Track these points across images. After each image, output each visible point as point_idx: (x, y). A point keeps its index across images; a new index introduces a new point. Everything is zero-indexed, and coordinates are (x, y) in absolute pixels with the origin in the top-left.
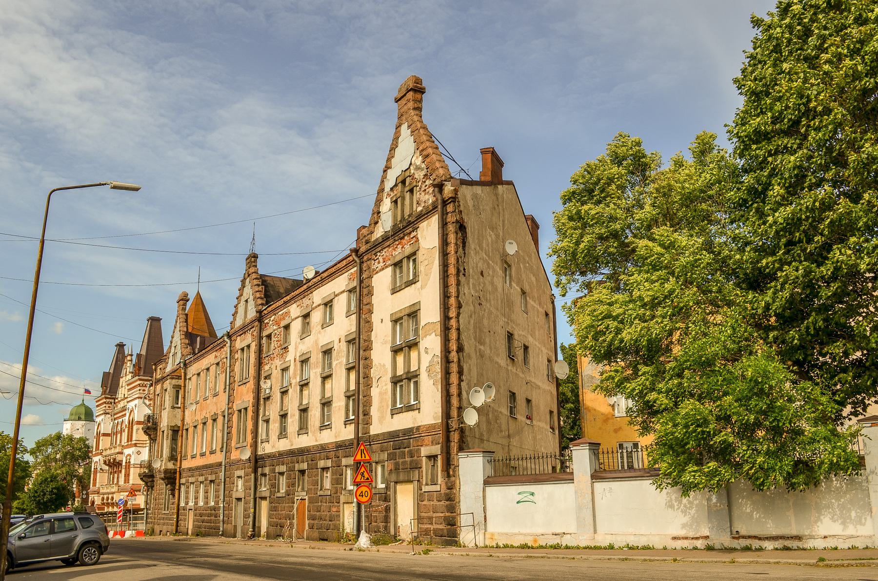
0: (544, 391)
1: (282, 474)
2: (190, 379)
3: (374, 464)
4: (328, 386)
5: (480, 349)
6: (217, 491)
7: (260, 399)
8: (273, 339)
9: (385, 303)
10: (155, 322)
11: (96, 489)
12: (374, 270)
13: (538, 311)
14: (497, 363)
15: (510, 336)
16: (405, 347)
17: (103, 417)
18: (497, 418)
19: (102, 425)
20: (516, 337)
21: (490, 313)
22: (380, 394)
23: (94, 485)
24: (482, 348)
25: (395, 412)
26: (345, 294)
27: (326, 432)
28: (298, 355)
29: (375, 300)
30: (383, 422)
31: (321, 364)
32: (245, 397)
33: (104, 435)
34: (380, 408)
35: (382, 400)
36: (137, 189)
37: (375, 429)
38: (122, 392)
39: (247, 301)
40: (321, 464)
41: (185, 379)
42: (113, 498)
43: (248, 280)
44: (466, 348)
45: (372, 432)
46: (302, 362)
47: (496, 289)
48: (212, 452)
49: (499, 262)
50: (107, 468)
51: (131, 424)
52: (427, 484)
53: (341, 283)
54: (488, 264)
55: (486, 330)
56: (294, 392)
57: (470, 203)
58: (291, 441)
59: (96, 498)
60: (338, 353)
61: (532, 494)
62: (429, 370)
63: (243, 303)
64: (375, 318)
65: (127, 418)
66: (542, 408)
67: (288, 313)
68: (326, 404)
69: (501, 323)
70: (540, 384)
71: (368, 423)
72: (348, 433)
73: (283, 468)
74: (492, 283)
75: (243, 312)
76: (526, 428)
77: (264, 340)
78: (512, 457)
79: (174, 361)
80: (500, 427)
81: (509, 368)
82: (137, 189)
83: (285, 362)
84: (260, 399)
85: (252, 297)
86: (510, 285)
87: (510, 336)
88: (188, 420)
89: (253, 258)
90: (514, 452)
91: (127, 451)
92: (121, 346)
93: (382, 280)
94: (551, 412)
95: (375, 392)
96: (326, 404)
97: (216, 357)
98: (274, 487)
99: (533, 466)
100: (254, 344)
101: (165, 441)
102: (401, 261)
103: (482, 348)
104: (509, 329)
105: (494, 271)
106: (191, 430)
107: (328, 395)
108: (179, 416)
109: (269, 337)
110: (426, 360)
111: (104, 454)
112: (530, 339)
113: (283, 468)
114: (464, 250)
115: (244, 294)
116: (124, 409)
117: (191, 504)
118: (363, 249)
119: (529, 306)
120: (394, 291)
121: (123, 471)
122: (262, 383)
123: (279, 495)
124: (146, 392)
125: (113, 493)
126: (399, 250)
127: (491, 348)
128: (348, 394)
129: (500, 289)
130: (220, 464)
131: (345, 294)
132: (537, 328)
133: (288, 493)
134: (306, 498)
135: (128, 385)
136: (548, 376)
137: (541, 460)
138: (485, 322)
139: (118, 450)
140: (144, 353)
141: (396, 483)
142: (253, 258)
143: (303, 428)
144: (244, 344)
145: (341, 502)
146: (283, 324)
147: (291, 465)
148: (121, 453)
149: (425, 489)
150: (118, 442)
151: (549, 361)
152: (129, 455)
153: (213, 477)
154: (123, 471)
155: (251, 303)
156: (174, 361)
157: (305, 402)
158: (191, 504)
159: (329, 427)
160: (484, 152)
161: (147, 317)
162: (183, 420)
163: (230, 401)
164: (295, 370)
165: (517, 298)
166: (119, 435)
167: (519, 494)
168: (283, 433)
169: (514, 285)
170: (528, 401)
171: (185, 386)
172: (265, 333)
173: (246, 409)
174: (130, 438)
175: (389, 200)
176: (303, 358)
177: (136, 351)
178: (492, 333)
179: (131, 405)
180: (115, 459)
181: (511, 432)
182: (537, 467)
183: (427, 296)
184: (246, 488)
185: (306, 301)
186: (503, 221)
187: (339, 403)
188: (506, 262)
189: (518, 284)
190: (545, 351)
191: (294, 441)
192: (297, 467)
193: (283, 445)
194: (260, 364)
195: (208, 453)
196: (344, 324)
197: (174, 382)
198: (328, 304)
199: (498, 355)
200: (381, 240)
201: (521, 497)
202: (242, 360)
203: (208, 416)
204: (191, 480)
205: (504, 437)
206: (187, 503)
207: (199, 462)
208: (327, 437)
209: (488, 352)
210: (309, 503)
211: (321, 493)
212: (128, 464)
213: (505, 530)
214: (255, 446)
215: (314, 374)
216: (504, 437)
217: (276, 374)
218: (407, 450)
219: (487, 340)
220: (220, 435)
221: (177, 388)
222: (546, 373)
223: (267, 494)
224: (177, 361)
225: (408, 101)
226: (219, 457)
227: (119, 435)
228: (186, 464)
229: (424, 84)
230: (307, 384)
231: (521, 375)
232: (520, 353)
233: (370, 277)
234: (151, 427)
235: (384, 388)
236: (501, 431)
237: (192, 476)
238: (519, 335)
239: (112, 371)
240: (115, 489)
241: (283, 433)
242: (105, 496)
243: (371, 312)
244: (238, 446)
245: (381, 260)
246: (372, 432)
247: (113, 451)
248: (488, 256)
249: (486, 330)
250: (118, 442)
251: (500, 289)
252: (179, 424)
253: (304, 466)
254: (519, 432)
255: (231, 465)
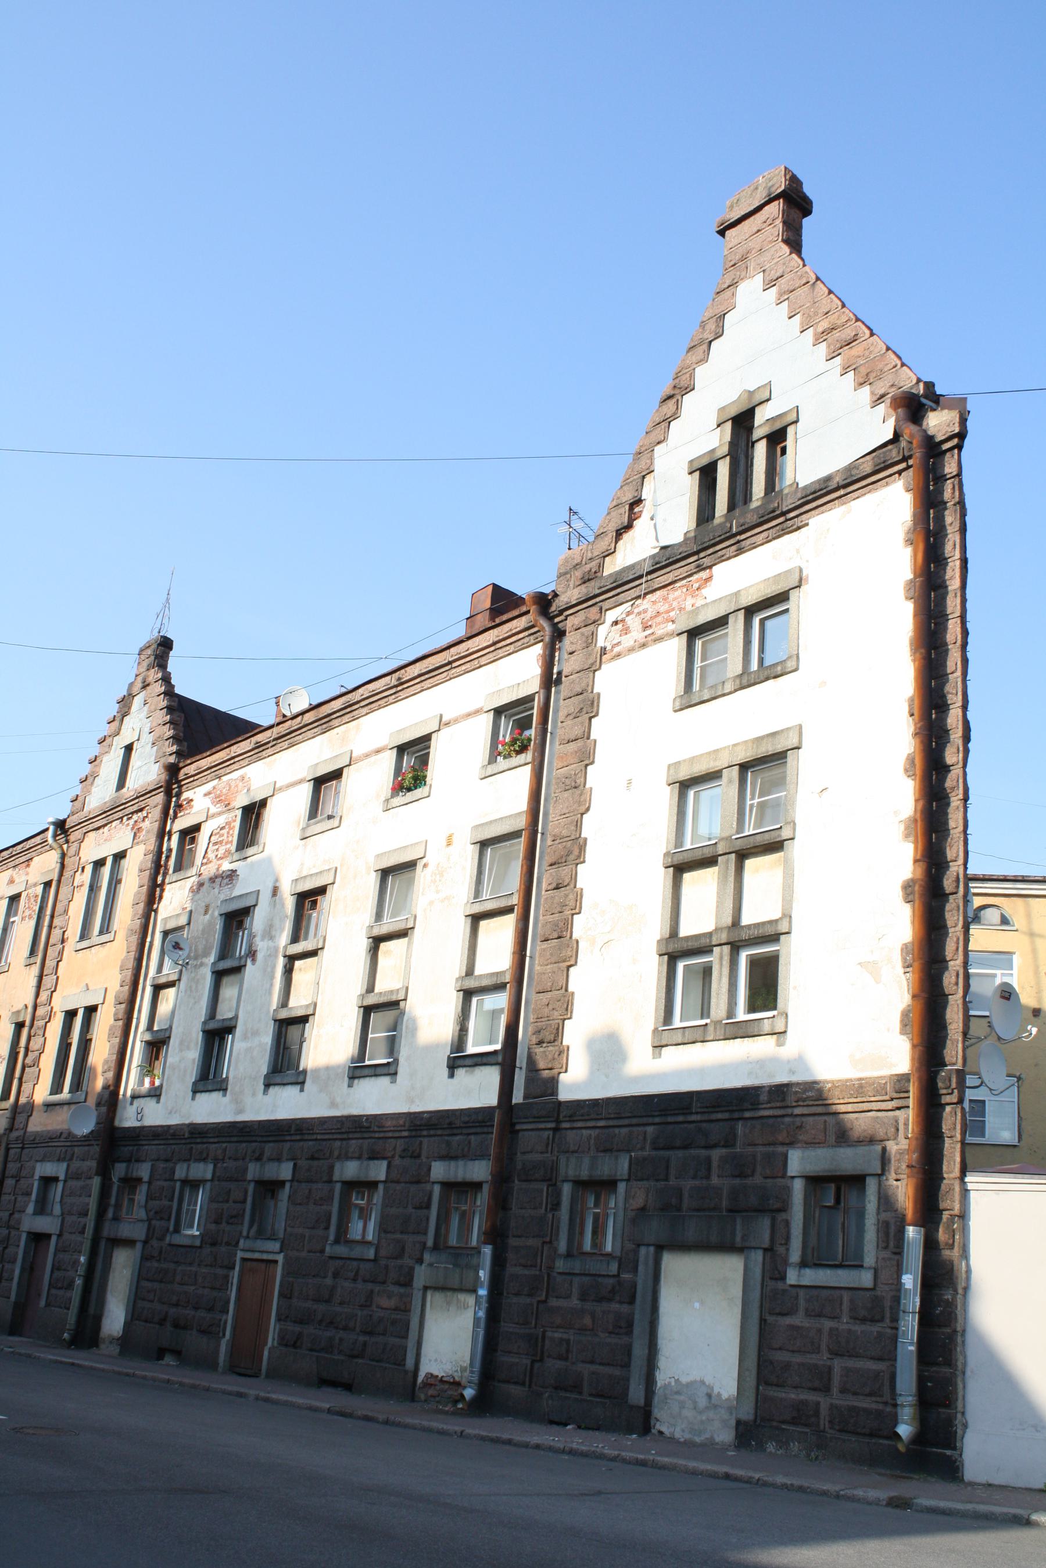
1: (193, 1185)
3: (567, 1189)
4: (229, 992)
12: (604, 651)
39: (129, 748)
40: (350, 1170)
43: (138, 701)
46: (385, 873)
52: (804, 1264)
58: (237, 1101)
97: (11, 881)
98: (165, 1216)
107: (224, 1012)
109: (190, 833)
113: (203, 1170)
118: (570, 595)
123: (177, 1240)
128: (471, 984)
133: (209, 1240)
134: (280, 1258)
141: (660, 1248)
144: (107, 850)
145: (419, 1281)
147: (230, 1164)
172: (183, 822)
173: (91, 1010)
192: (180, 1172)
193: (210, 1110)
196: (477, 792)
200: (647, 568)
210: (286, 1273)
211: (341, 1250)
218: (716, 1154)
223: (138, 1232)
229: (808, 190)
230: (238, 970)
243: (586, 758)
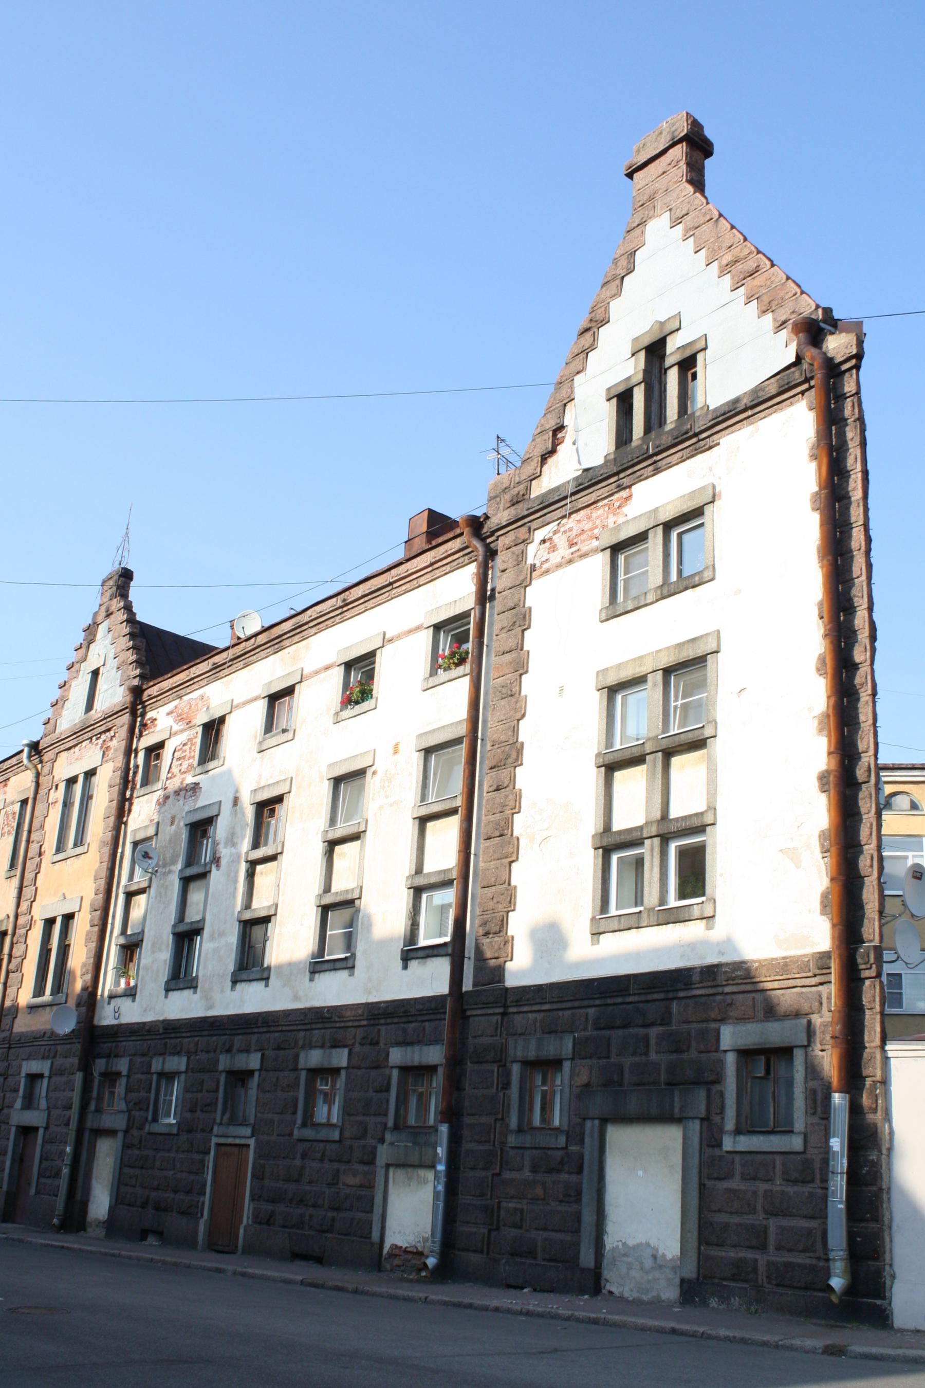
134: (252, 1142)
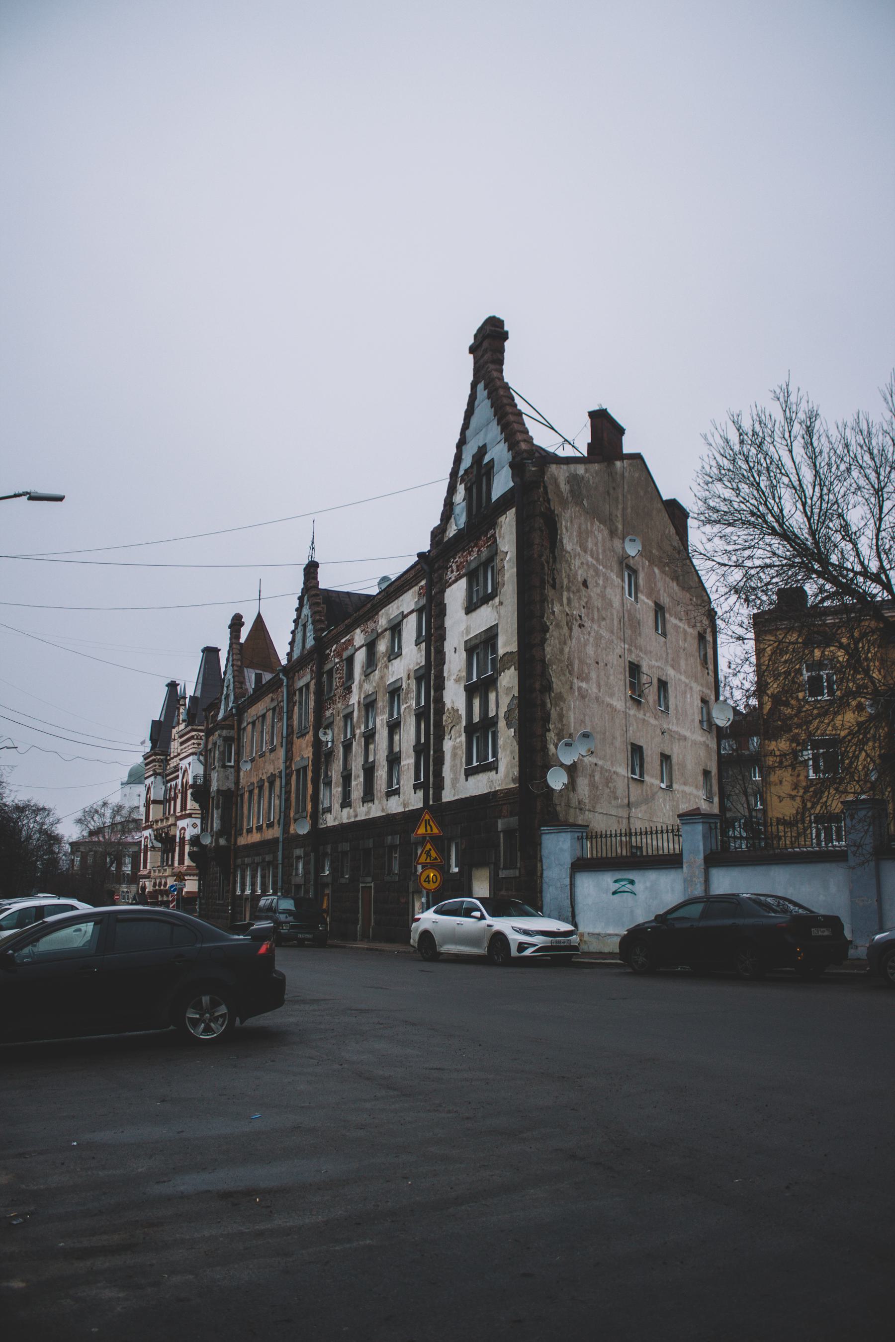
0: (695, 743)
2: (244, 729)
5: (580, 688)
6: (275, 876)
7: (322, 756)
8: (335, 676)
9: (460, 626)
10: (210, 653)
11: (146, 872)
13: (685, 632)
14: (611, 706)
15: (634, 669)
16: (479, 688)
17: (152, 779)
18: (608, 781)
19: (152, 789)
20: (645, 669)
21: (598, 638)
22: (455, 748)
23: (145, 867)
24: (584, 685)
25: (470, 772)
26: (414, 615)
27: (394, 800)
28: (362, 696)
29: (448, 622)
30: (459, 786)
31: (387, 710)
32: (304, 750)
33: (155, 802)
34: (453, 767)
35: (454, 755)
36: (60, 499)
37: (448, 796)
38: (175, 746)
41: (239, 729)
42: (166, 884)
44: (555, 686)
45: (444, 800)
47: (611, 605)
48: (270, 825)
49: (616, 567)
50: (160, 845)
51: (185, 787)
52: (505, 868)
53: (408, 601)
54: (597, 571)
55: (591, 661)
56: (357, 748)
57: (564, 487)
58: (355, 811)
59: (147, 883)
60: (407, 693)
61: (632, 882)
62: (507, 716)
63: (300, 628)
64: (448, 647)
65: (179, 781)
66: (690, 765)
67: (350, 642)
68: (394, 760)
69: (618, 651)
70: (688, 734)
71: (439, 785)
72: (414, 800)
73: (346, 847)
74: (603, 596)
75: (301, 641)
76: (660, 794)
77: (325, 678)
78: (633, 831)
79: (227, 705)
80: (614, 792)
81: (632, 712)
82: (60, 499)
83: (348, 706)
84: (322, 756)
85: (310, 620)
86: (636, 598)
87: (634, 669)
88: (243, 782)
89: (311, 569)
90: (637, 825)
91: (181, 824)
92: (172, 686)
93: (456, 594)
94: (706, 773)
95: (448, 745)
96: (394, 760)
97: (272, 700)
99: (660, 844)
100: (313, 682)
101: (215, 811)
102: (476, 569)
103: (584, 685)
104: (633, 658)
105: (606, 579)
106: (246, 795)
108: (232, 778)
110: (505, 702)
111: (155, 827)
112: (671, 672)
113: (346, 847)
114: (553, 552)
115: (302, 616)
116: (176, 769)
117: (248, 892)
119: (669, 627)
120: (470, 608)
121: (177, 848)
122: (321, 734)
123: (343, 881)
124: (202, 746)
125: (166, 877)
126: (475, 554)
127: (599, 686)
129: (616, 603)
130: (275, 841)
131: (414, 615)
132: (682, 655)
134: (372, 885)
135: (181, 737)
136: (701, 722)
137: (659, 836)
138: (590, 650)
139: (171, 821)
140: (198, 694)
142: (311, 569)
143: (368, 796)
145: (411, 890)
146: (345, 655)
148: (175, 825)
149: (503, 874)
150: (172, 812)
151: (704, 701)
152: (183, 828)
153: (268, 858)
154: (177, 848)
155: (310, 627)
156: (227, 705)
157: (371, 759)
158: (248, 892)
159: (397, 792)
160: (593, 415)
161: (202, 648)
162: (237, 782)
163: (289, 758)
164: (359, 717)
165: (648, 619)
166: (172, 803)
167: (616, 881)
168: (346, 803)
169: (642, 597)
170: (666, 758)
171: (239, 739)
174: (184, 807)
175: (463, 486)
176: (368, 700)
177: (190, 692)
178: (601, 664)
179: (184, 764)
180: (167, 834)
181: (632, 799)
182: (665, 844)
183: (500, 616)
184: (306, 872)
185: (371, 625)
186: (624, 509)
187: (408, 761)
188: (628, 567)
189: (649, 596)
190: (696, 688)
191: (358, 810)
194: (320, 709)
195: (265, 825)
196: (412, 655)
197: (225, 733)
198: (395, 629)
199: (612, 695)
201: (617, 885)
202: (301, 703)
203: (264, 777)
204: (247, 860)
205: (621, 806)
206: (243, 890)
207: (256, 837)
208: (395, 806)
209: (595, 690)
212: (182, 839)
213: (597, 931)
214: (315, 818)
215: (381, 721)
216: (621, 806)
217: (339, 722)
219: (593, 675)
220: (277, 802)
221: (228, 740)
222: (697, 718)
224: (231, 705)
225: (485, 351)
226: (275, 832)
227: (172, 803)
228: (242, 841)
231: (653, 721)
232: (651, 694)
233: (443, 592)
234: (201, 792)
235: (458, 740)
236: (616, 798)
237: (248, 856)
238: (651, 667)
239: (162, 719)
240: (169, 872)
241: (346, 803)
242: (158, 881)
244: (297, 816)
245: (454, 568)
246: (444, 800)
247: (165, 824)
248: (597, 560)
249: (591, 661)
250: (172, 812)
251: (616, 603)
252: (232, 786)
253: (370, 843)
254: (648, 799)
255: (291, 841)
